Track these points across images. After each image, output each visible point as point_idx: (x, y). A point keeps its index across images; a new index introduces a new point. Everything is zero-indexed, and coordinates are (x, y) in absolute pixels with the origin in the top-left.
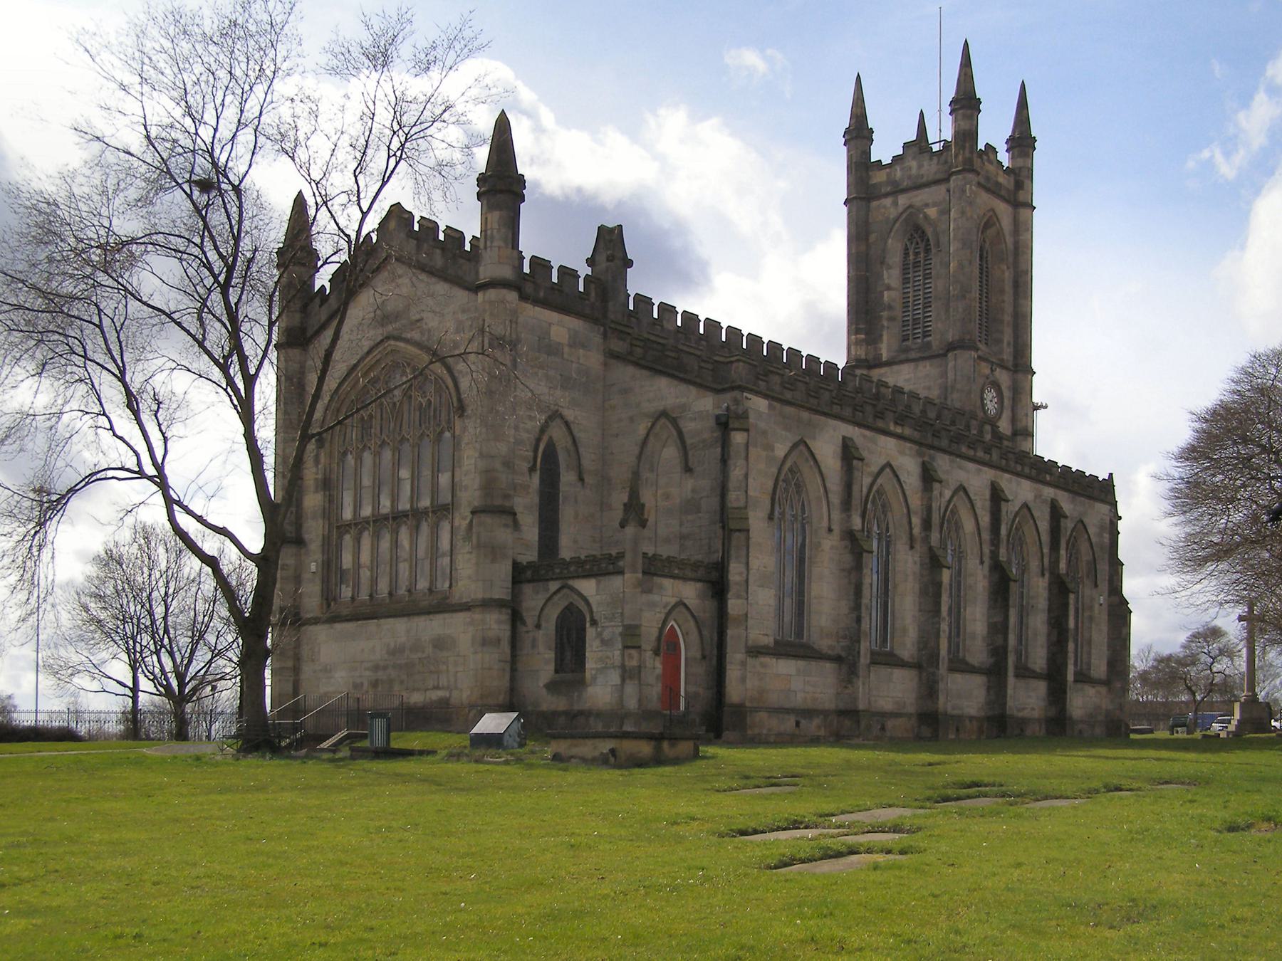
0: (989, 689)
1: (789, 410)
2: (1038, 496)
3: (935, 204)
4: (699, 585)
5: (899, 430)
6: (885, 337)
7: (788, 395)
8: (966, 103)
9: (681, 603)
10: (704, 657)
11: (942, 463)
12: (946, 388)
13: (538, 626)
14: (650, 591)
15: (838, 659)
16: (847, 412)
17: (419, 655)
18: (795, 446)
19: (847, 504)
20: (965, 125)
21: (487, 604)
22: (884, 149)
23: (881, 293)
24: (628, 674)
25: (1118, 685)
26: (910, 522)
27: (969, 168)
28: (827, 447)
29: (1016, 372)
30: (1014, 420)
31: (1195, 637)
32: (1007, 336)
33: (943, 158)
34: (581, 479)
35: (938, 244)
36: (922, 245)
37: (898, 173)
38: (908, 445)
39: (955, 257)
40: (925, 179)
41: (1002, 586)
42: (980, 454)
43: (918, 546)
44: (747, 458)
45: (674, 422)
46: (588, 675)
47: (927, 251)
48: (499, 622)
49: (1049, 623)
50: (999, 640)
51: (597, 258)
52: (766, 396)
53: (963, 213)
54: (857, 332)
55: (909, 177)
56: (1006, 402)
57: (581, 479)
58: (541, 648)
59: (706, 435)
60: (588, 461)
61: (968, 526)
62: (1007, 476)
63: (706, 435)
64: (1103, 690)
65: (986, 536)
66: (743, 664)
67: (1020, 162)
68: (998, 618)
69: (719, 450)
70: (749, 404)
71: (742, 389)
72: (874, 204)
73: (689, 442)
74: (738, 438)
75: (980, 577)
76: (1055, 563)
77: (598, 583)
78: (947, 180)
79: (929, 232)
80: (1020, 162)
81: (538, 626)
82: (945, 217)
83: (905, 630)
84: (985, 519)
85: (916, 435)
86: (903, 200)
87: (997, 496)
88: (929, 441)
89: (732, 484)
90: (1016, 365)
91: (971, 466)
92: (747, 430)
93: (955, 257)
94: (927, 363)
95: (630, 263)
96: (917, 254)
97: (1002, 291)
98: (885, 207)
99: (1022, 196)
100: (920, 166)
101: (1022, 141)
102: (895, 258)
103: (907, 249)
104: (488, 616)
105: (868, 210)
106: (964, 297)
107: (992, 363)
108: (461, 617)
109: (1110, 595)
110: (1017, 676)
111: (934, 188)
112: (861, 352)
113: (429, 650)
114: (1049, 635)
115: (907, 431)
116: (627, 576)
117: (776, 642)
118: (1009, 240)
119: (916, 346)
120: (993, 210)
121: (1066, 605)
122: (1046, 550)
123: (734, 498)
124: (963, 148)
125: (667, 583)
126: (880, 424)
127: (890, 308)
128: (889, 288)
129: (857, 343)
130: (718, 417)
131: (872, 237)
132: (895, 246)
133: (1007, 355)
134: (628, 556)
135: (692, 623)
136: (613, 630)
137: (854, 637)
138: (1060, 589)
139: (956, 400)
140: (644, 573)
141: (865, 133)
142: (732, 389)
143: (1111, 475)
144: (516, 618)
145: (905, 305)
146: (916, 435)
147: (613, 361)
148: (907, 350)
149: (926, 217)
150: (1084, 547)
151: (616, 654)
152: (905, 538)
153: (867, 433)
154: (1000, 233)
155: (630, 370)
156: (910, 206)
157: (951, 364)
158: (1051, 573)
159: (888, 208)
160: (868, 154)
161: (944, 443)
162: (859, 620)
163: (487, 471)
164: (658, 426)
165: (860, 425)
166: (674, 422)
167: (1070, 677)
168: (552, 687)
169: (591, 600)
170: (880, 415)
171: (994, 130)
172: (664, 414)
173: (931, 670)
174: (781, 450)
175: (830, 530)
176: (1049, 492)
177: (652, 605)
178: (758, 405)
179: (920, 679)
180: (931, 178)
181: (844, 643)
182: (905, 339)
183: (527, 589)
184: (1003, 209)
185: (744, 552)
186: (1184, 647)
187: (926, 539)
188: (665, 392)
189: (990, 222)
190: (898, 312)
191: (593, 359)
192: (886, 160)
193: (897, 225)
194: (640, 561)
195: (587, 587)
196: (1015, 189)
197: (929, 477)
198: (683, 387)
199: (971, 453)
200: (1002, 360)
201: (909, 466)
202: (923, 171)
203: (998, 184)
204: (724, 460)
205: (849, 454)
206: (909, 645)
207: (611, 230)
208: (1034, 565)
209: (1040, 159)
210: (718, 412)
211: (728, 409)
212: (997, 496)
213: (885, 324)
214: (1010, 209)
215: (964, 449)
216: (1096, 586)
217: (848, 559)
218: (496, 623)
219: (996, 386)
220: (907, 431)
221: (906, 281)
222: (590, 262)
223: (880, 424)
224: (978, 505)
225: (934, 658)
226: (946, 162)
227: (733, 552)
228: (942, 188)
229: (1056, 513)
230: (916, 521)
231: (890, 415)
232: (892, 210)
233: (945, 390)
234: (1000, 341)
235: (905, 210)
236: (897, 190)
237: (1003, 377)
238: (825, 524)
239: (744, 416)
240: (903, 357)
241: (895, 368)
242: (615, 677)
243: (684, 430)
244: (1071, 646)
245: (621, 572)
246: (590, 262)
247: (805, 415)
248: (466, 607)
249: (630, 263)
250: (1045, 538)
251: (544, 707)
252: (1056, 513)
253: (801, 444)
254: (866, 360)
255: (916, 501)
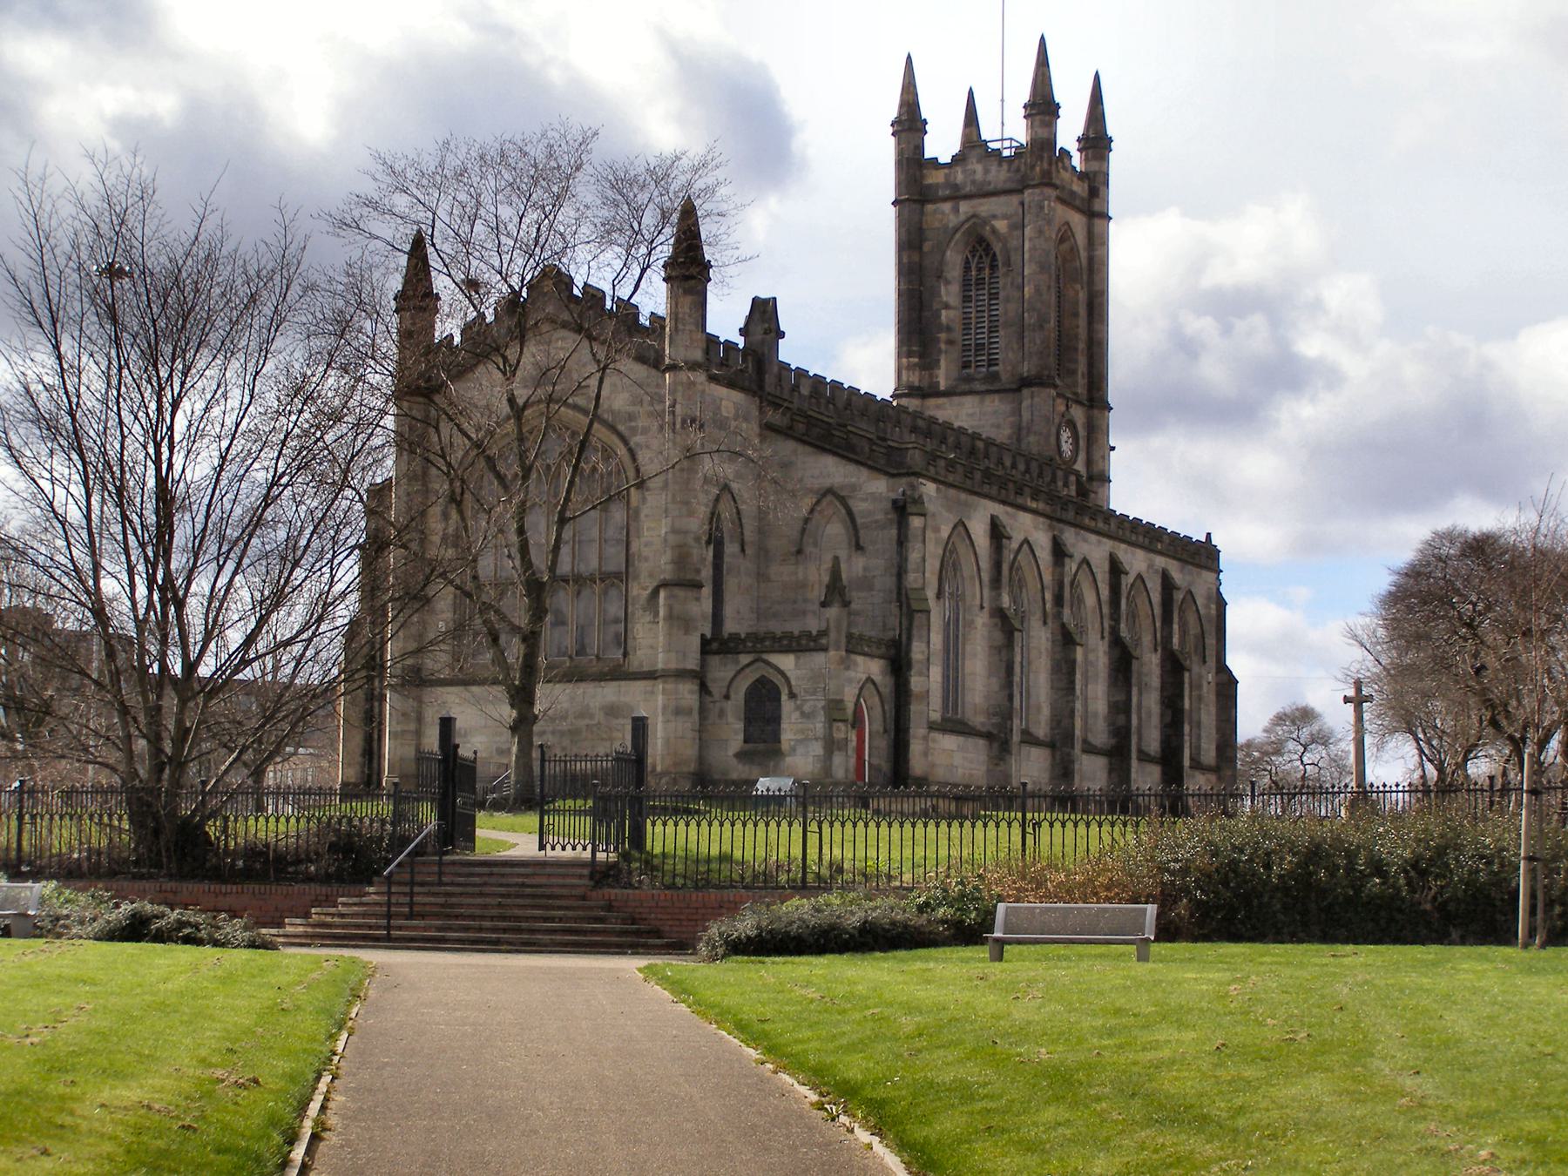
0: (1110, 771)
1: (952, 492)
2: (1150, 566)
3: (1005, 217)
4: (882, 662)
5: (1034, 505)
6: (943, 363)
7: (951, 478)
8: (1042, 107)
9: (869, 680)
10: (885, 731)
11: (1069, 536)
12: (1020, 429)
13: (727, 697)
14: (848, 668)
15: (988, 736)
16: (994, 491)
17: (587, 721)
18: (955, 527)
19: (996, 582)
20: (1043, 133)
21: (680, 674)
22: (942, 143)
23: (938, 311)
24: (831, 745)
25: (1229, 773)
26: (1044, 599)
27: (1047, 181)
28: (979, 530)
29: (1091, 407)
30: (1089, 463)
31: (1280, 719)
32: (1082, 367)
33: (1014, 166)
34: (743, 550)
35: (1008, 263)
36: (987, 261)
37: (959, 176)
38: (1041, 519)
39: (1030, 277)
40: (991, 187)
41: (1123, 664)
42: (1101, 525)
43: (1049, 621)
44: (924, 541)
45: (843, 501)
46: (785, 746)
47: (993, 267)
48: (691, 692)
49: (1162, 703)
50: (1121, 720)
51: (751, 328)
52: (934, 480)
53: (1041, 232)
54: (909, 354)
55: (973, 182)
56: (1082, 443)
57: (743, 550)
58: (731, 719)
59: (880, 516)
60: (749, 534)
61: (1090, 599)
62: (1123, 546)
63: (880, 516)
64: (1213, 778)
65: (1106, 610)
66: (925, 738)
67: (1095, 166)
68: (1121, 697)
69: (894, 532)
70: (923, 489)
71: (917, 475)
72: (929, 207)
73: (859, 521)
74: (916, 522)
75: (1101, 654)
76: (1167, 638)
77: (797, 658)
78: (1021, 191)
79: (997, 248)
80: (1095, 166)
81: (727, 697)
82: (1018, 233)
83: (1039, 709)
84: (1105, 592)
85: (1048, 509)
86: (964, 207)
87: (1116, 569)
88: (1058, 515)
89: (911, 566)
90: (1091, 399)
91: (1093, 538)
92: (924, 515)
93: (1030, 277)
94: (996, 397)
95: (782, 335)
96: (980, 270)
97: (1076, 315)
98: (943, 213)
99: (1097, 207)
100: (986, 171)
101: (1096, 140)
102: (954, 271)
103: (967, 262)
104: (681, 686)
105: (922, 213)
106: (1041, 327)
107: (1068, 399)
108: (640, 685)
109: (1217, 673)
110: (1140, 760)
111: (1003, 199)
112: (914, 378)
113: (600, 717)
114: (1162, 715)
115: (1041, 506)
116: (832, 653)
117: (943, 719)
118: (1083, 254)
119: (980, 375)
120: (1067, 223)
121: (1182, 683)
122: (1158, 624)
123: (912, 579)
124: (1041, 158)
125: (860, 659)
126: (1020, 500)
127: (949, 329)
128: (947, 307)
129: (910, 367)
130: (895, 502)
131: (927, 247)
132: (954, 259)
133: (1081, 390)
134: (833, 635)
135: (877, 699)
136: (816, 703)
137: (1004, 714)
138: (1174, 667)
139: (1032, 443)
140: (847, 651)
141: (919, 125)
142: (908, 474)
143: (1209, 535)
144: (704, 689)
145: (966, 327)
146: (1048, 509)
147: (768, 433)
148: (969, 379)
149: (994, 231)
150: (1192, 619)
151: (819, 726)
152: (1039, 614)
153: (1009, 509)
154: (1074, 250)
155: (791, 445)
156: (974, 216)
157: (1025, 404)
158: (1164, 649)
159: (945, 214)
160: (920, 148)
161: (1070, 515)
162: (1011, 697)
163: (680, 546)
164: (825, 502)
165: (1004, 502)
166: (843, 501)
167: (1187, 762)
168: (740, 755)
169: (789, 674)
170: (1019, 492)
171: (1069, 131)
172: (830, 491)
173: (1066, 750)
174: (945, 533)
175: (982, 607)
176: (1160, 562)
177: (850, 681)
178: (929, 489)
179: (1053, 757)
180: (1000, 186)
181: (995, 720)
182: (966, 365)
183: (714, 661)
184: (1077, 221)
185: (925, 633)
186: (1265, 731)
187: (1058, 615)
188: (831, 470)
189: (1066, 235)
190: (957, 335)
191: (751, 429)
192: (945, 158)
193: (958, 236)
194: (844, 640)
195: (786, 662)
196: (1090, 197)
197: (1059, 552)
198: (852, 468)
199: (1093, 524)
200: (1076, 394)
201: (1042, 540)
202: (990, 177)
203: (1073, 193)
204: (902, 542)
205: (997, 532)
206: (1043, 724)
207: (766, 301)
208: (1147, 639)
209: (1119, 163)
210: (893, 496)
211: (904, 493)
212: (1116, 569)
213: (943, 346)
214: (1084, 219)
215: (1087, 521)
216: (1205, 662)
217: (999, 637)
218: (687, 693)
219: (1071, 424)
220: (1041, 506)
221: (966, 299)
222: (743, 332)
223: (1020, 500)
224: (1099, 577)
225: (1069, 737)
226: (1018, 170)
227: (915, 632)
228: (1015, 199)
229: (1168, 585)
230: (1048, 596)
231: (1027, 491)
232: (952, 217)
233: (1019, 431)
234: (1073, 372)
235: (967, 220)
236: (956, 195)
237: (1078, 414)
238: (978, 602)
239: (919, 501)
240: (965, 387)
241: (956, 399)
242: (817, 749)
243: (854, 509)
244: (1187, 728)
245: (825, 649)
246: (743, 332)
247: (963, 496)
248: (651, 676)
249: (782, 335)
250: (1158, 611)
251: (734, 776)
252: (1168, 585)
253: (961, 525)
254: (919, 388)
255: (1047, 578)
